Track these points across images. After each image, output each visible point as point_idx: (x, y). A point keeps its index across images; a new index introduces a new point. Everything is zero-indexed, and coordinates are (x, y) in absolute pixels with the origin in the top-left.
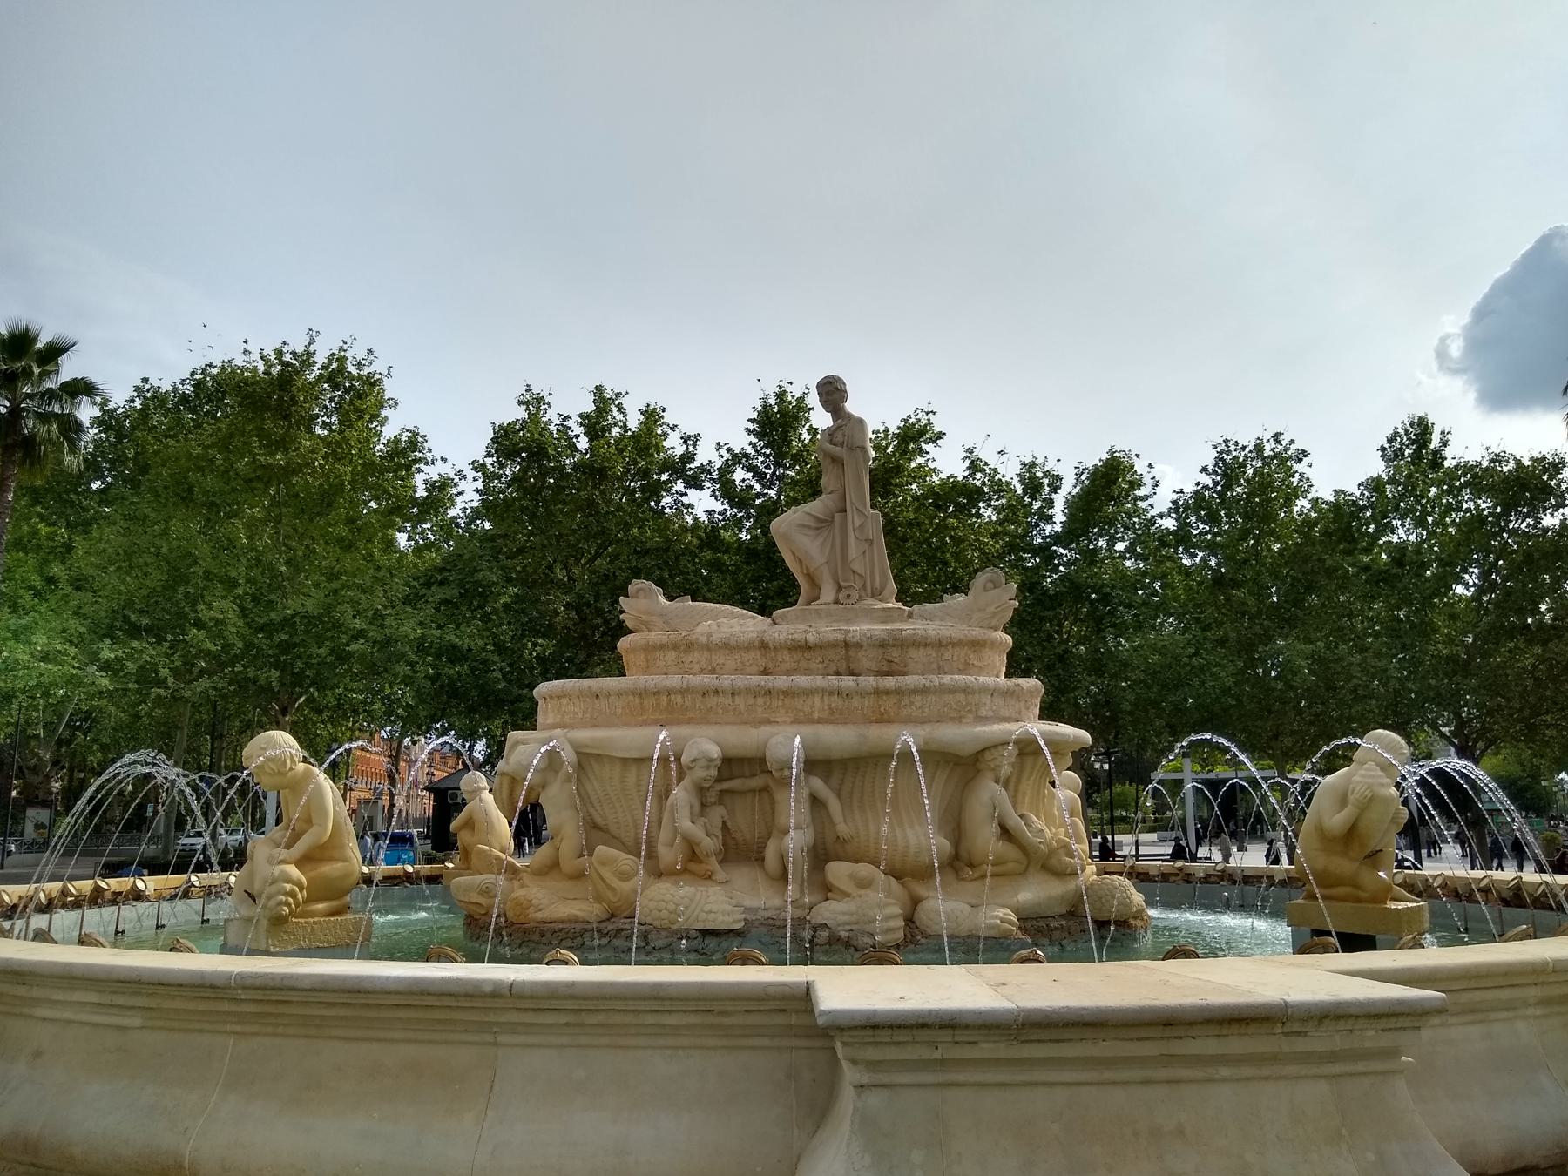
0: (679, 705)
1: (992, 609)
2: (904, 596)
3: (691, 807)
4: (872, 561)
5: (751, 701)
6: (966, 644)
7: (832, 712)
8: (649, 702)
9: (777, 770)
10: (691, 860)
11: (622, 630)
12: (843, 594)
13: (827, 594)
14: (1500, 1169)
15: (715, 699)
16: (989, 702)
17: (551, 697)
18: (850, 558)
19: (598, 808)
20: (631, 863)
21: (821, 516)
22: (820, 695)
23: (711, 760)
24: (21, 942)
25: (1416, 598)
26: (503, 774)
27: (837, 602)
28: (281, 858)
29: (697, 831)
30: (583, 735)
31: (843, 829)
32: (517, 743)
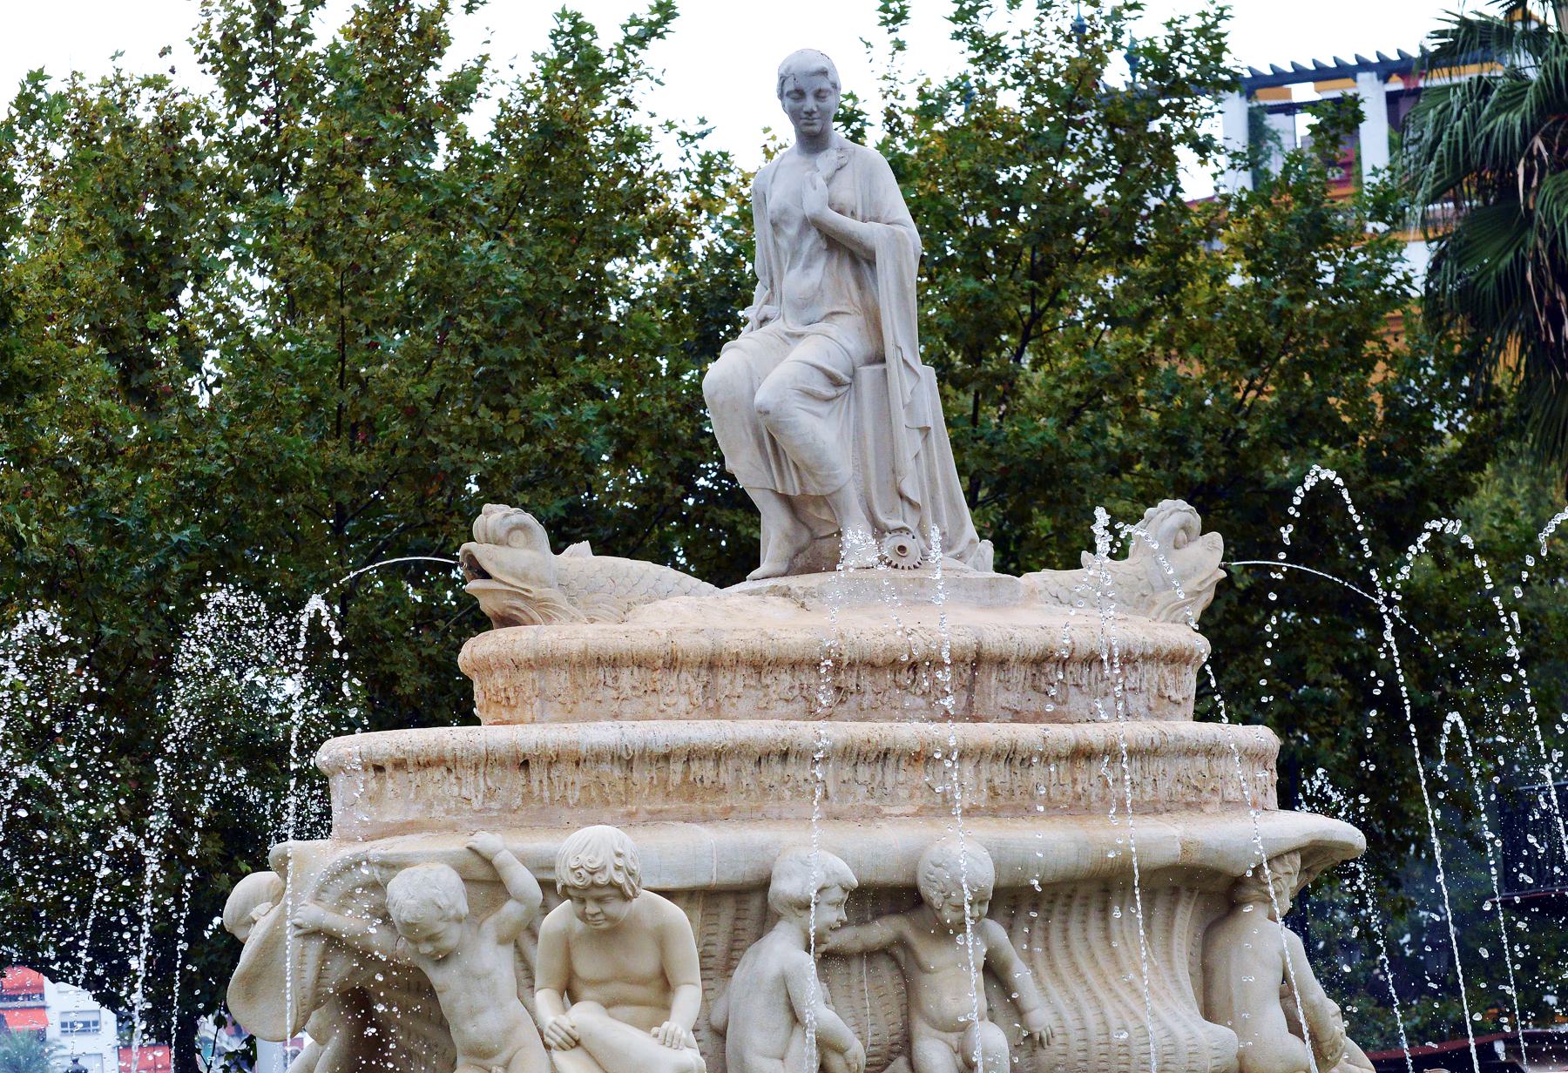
2: (1012, 559)
4: (930, 467)
5: (847, 773)
7: (994, 793)
8: (641, 775)
13: (857, 539)
15: (778, 768)
22: (975, 761)
24: (655, 1041)
25: (1419, 382)
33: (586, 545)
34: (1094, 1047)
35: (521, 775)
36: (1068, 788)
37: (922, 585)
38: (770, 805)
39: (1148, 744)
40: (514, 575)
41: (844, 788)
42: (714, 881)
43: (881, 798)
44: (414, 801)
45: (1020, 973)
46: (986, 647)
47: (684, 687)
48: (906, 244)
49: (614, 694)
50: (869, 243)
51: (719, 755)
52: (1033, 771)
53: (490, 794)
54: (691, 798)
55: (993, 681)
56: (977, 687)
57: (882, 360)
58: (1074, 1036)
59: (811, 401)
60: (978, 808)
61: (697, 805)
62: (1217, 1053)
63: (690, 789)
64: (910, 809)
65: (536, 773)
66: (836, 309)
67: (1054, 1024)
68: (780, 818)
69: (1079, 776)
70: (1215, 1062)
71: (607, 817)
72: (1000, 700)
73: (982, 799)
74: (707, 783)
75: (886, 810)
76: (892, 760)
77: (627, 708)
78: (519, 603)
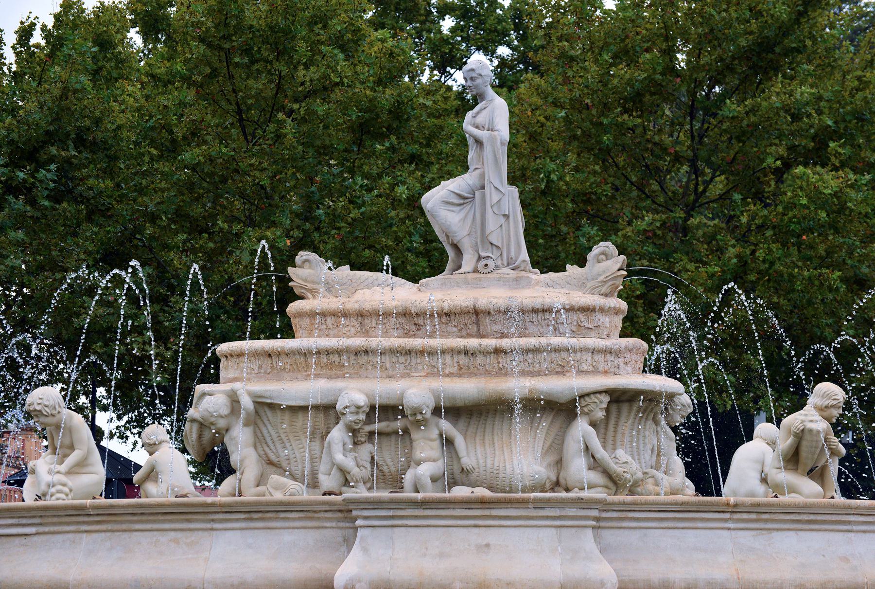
0: (336, 363)
1: (602, 278)
3: (344, 444)
6: (578, 310)
7: (460, 368)
9: (411, 415)
10: (344, 485)
11: (293, 296)
12: (483, 262)
14: (683, 585)
15: (366, 357)
16: (589, 359)
17: (232, 356)
18: (488, 232)
19: (272, 447)
20: (298, 488)
21: (466, 195)
23: (359, 407)
26: (193, 420)
27: (476, 271)
28: (56, 470)
29: (348, 462)
30: (259, 387)
31: (467, 461)
32: (204, 395)
33: (348, 266)
34: (488, 474)
35: (269, 360)
36: (496, 366)
37: (480, 280)
38: (363, 372)
39: (533, 347)
40: (302, 279)
41: (394, 365)
42: (319, 403)
43: (410, 369)
44: (237, 369)
45: (460, 441)
46: (477, 306)
47: (352, 324)
48: (496, 139)
49: (325, 326)
50: (481, 139)
51: (339, 352)
52: (478, 358)
53: (260, 367)
54: (331, 369)
55: (487, 320)
56: (480, 323)
57: (483, 188)
58: (482, 469)
59: (448, 205)
60: (453, 374)
61: (334, 372)
62: (532, 478)
63: (331, 366)
64: (423, 374)
65: (275, 359)
66: (477, 167)
67: (476, 467)
68: (366, 377)
69: (500, 361)
70: (532, 482)
71: (299, 376)
72: (493, 328)
73: (455, 370)
74: (336, 363)
75: (412, 374)
76: (413, 354)
77: (332, 333)
78: (303, 291)
